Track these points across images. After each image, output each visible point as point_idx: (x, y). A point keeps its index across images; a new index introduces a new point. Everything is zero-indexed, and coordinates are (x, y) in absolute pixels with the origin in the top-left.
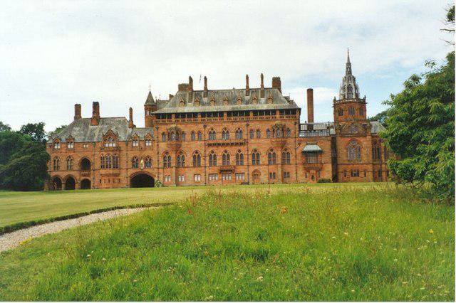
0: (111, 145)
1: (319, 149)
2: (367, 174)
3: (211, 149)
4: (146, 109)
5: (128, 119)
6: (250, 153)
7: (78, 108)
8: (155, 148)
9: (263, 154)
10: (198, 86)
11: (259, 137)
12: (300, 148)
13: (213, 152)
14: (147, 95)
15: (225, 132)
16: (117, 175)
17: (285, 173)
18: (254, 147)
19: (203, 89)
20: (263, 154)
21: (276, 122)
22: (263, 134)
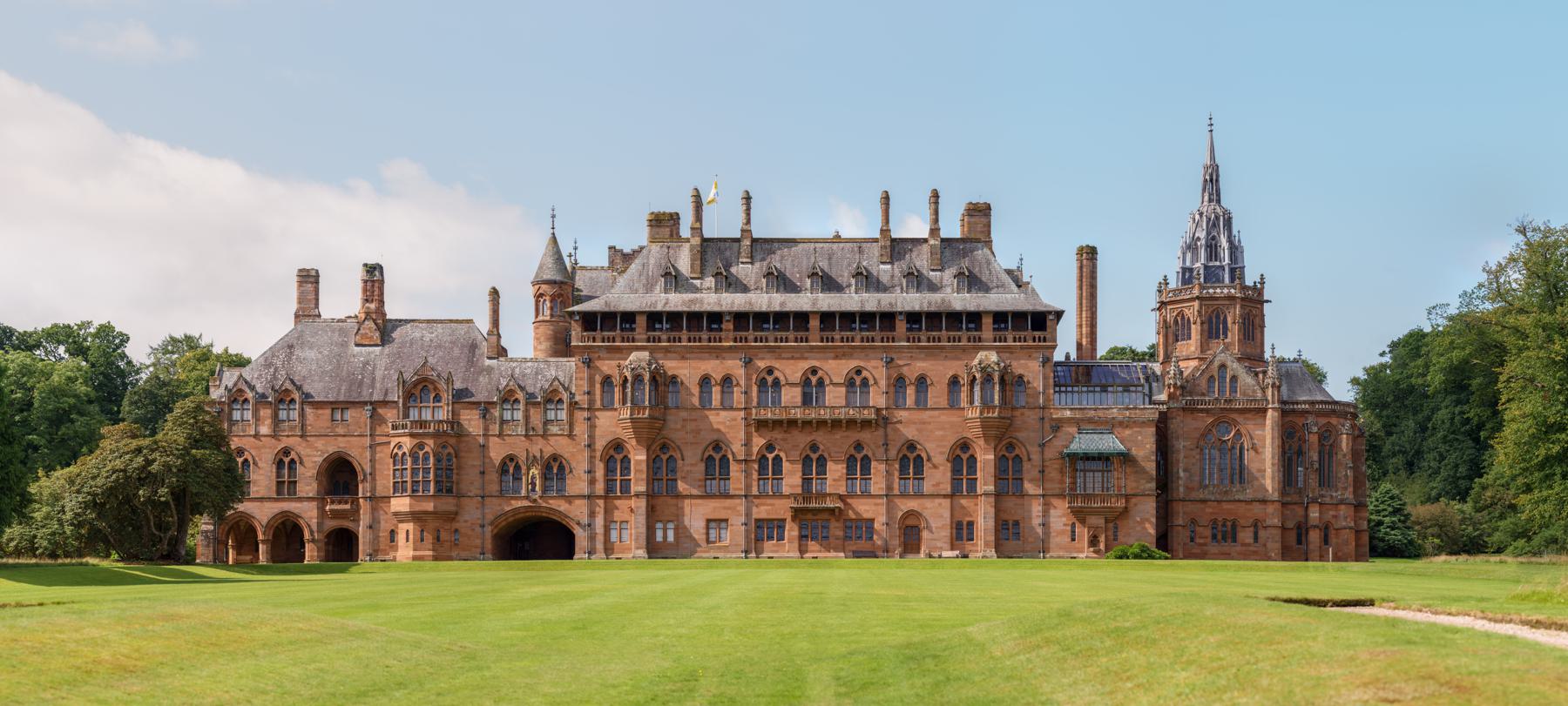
2: (1262, 533)
5: (484, 325)
7: (309, 279)
10: (722, 223)
11: (921, 404)
12: (1058, 443)
15: (812, 387)
16: (451, 517)
17: (1006, 523)
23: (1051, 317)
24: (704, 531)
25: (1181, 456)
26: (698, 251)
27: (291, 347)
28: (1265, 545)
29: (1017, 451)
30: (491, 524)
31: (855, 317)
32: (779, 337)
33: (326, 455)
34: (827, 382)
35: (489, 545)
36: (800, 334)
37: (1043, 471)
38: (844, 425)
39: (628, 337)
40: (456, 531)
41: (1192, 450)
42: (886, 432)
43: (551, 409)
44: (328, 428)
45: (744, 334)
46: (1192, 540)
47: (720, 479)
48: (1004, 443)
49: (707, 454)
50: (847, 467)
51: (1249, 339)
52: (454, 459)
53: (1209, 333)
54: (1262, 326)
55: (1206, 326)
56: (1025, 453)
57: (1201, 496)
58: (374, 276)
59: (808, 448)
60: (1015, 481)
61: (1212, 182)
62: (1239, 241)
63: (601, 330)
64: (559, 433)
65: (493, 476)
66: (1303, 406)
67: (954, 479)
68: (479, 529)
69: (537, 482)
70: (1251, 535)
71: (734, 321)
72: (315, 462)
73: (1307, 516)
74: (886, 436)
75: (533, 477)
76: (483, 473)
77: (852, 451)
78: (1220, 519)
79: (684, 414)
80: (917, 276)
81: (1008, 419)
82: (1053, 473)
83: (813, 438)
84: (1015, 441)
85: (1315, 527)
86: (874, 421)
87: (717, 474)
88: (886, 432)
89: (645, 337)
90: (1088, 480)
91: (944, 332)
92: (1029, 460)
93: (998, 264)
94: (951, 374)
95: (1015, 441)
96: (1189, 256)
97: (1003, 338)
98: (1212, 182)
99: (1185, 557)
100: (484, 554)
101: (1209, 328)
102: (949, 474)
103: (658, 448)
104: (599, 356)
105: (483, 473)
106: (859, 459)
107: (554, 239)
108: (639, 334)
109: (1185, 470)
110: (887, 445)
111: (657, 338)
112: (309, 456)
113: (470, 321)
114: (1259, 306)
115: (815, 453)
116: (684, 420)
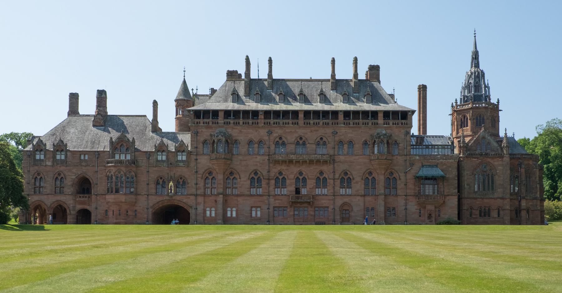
0: (123, 157)
1: (441, 173)
2: (501, 212)
3: (279, 168)
4: (177, 106)
5: (150, 117)
6: (337, 176)
7: (74, 98)
8: (192, 164)
9: (358, 179)
12: (413, 171)
13: (280, 173)
14: (380, 79)
18: (342, 167)
19: (329, 77)
20: (358, 179)
21: (379, 130)
22: (358, 146)
23: (410, 113)
24: (250, 212)
25: (466, 178)
26: (248, 84)
27: (64, 127)
28: (503, 218)
29: (394, 176)
30: (152, 207)
31: (320, 113)
32: (285, 122)
33: (77, 175)
34: (307, 143)
35: (150, 217)
36: (294, 121)
37: (406, 185)
38: (315, 163)
39: (215, 122)
40: (136, 211)
41: (470, 175)
42: (334, 166)
43: (180, 155)
44: (78, 163)
45: (268, 121)
46: (471, 215)
47: (257, 188)
48: (389, 171)
49: (251, 177)
50: (316, 183)
51: (493, 127)
52: (135, 178)
53: (476, 124)
54: (499, 121)
55: (475, 121)
56: (398, 176)
57: (475, 196)
58: (102, 96)
59: (298, 174)
60: (372, 189)
61: (476, 57)
62: (488, 84)
63: (203, 118)
64: (183, 166)
65: (153, 186)
66: (518, 156)
67: (39, 193)
68: (146, 210)
69: (173, 189)
70: (497, 213)
71: (264, 114)
72: (72, 178)
73: (520, 205)
74: (334, 168)
75: (171, 187)
76: (148, 184)
77: (319, 175)
78: (483, 206)
79: (240, 157)
80: (348, 95)
81: (390, 160)
82: (411, 185)
83: (300, 169)
84: (393, 171)
85: (524, 209)
86: (328, 161)
87: (281, 186)
88: (334, 166)
89: (223, 122)
90: (426, 188)
91: (361, 120)
92: (400, 179)
93: (384, 91)
94: (364, 139)
95: (393, 171)
96: (466, 91)
97: (388, 123)
98: (476, 57)
99: (468, 224)
100: (148, 221)
101: (476, 121)
102: (363, 186)
103: (229, 174)
104: (202, 131)
105: (148, 184)
106: (321, 179)
107: (184, 82)
108: (220, 120)
109: (467, 185)
110: (335, 172)
111: (228, 122)
112: (70, 176)
113: (145, 116)
114: (497, 112)
115: (301, 176)
116: (241, 160)
